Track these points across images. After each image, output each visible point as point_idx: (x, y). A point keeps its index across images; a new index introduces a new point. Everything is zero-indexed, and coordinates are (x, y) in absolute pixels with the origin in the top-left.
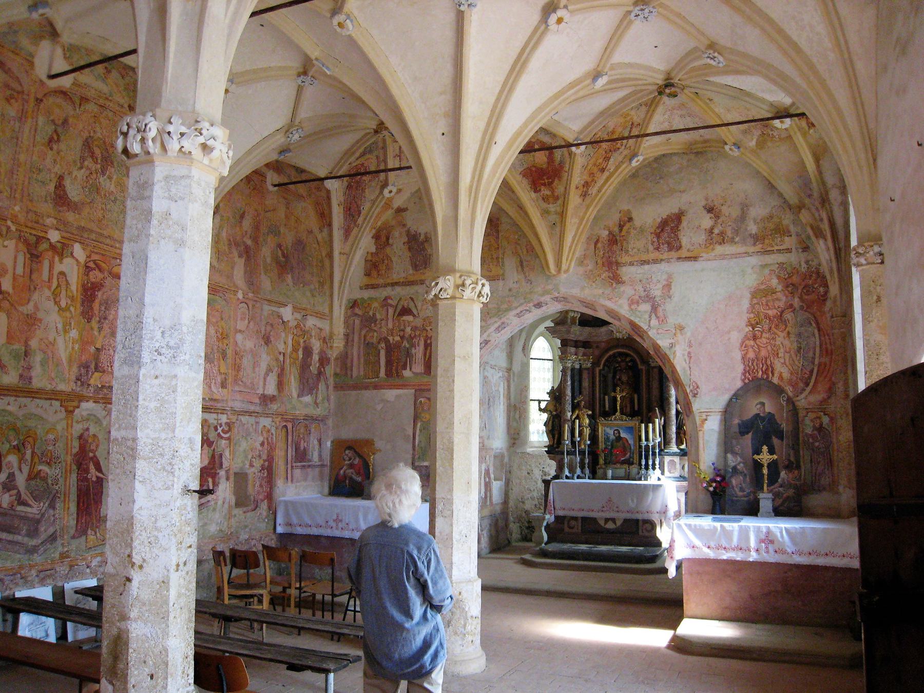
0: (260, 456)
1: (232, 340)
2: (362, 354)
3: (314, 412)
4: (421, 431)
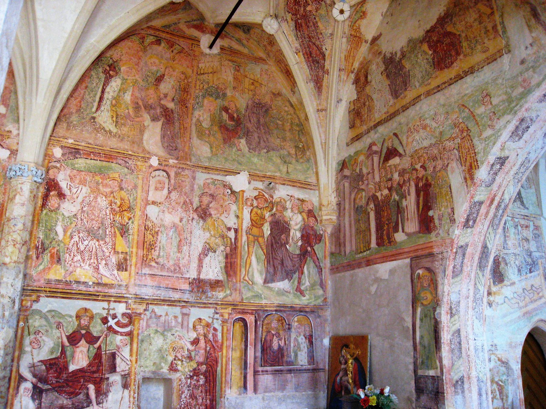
0: (190, 358)
1: (138, 213)
2: (353, 222)
3: (297, 301)
4: (421, 320)
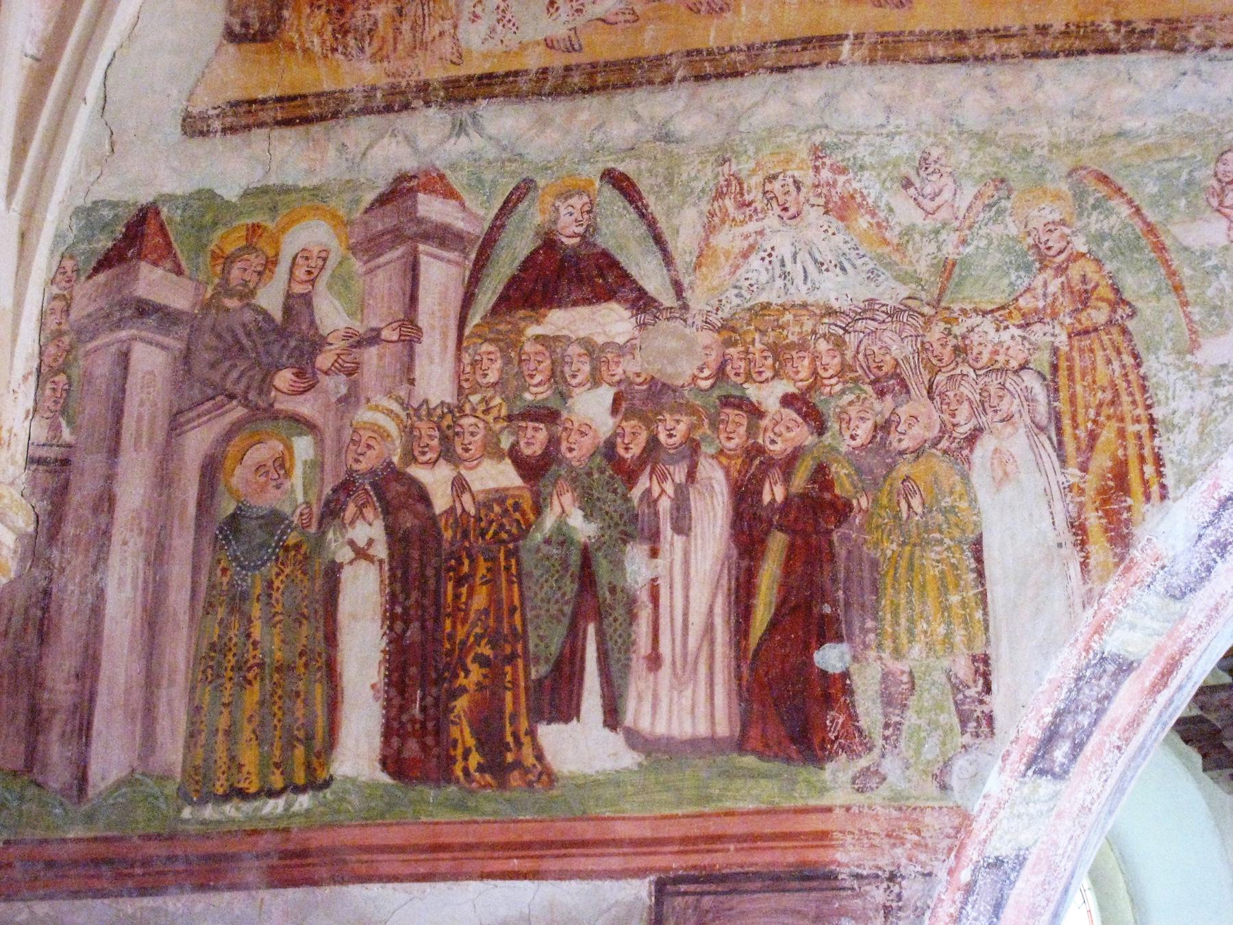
2: (178, 599)
